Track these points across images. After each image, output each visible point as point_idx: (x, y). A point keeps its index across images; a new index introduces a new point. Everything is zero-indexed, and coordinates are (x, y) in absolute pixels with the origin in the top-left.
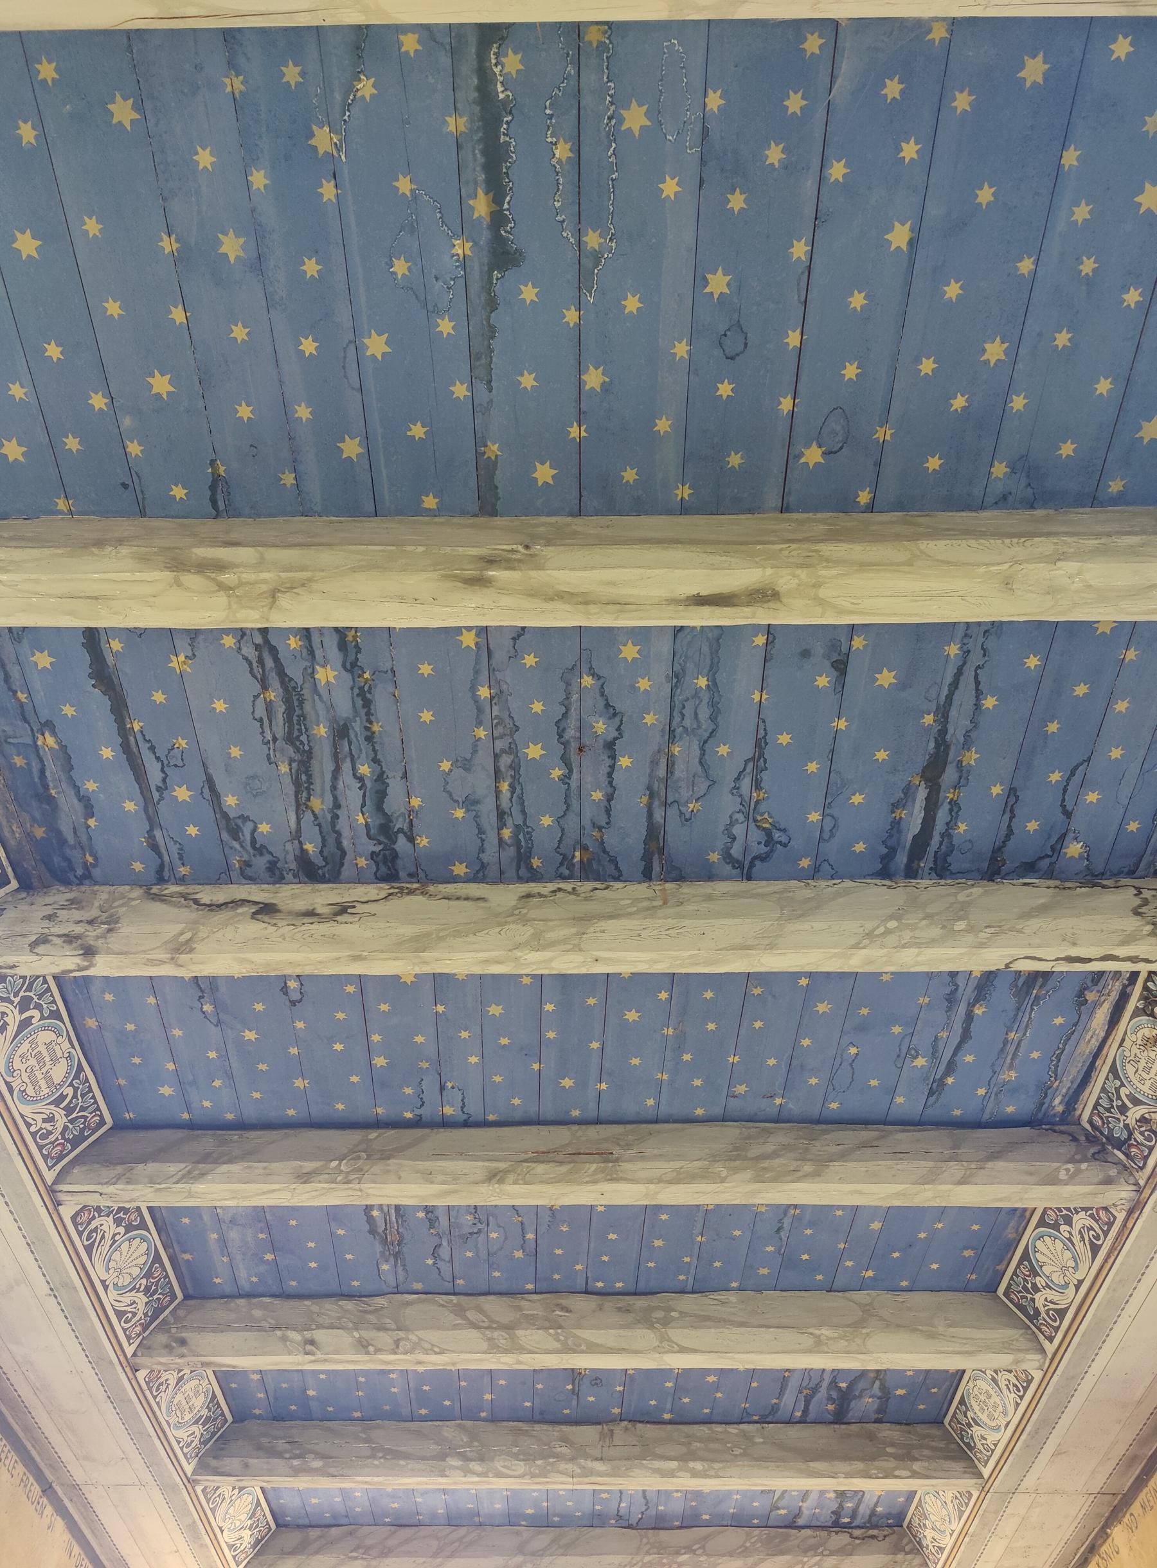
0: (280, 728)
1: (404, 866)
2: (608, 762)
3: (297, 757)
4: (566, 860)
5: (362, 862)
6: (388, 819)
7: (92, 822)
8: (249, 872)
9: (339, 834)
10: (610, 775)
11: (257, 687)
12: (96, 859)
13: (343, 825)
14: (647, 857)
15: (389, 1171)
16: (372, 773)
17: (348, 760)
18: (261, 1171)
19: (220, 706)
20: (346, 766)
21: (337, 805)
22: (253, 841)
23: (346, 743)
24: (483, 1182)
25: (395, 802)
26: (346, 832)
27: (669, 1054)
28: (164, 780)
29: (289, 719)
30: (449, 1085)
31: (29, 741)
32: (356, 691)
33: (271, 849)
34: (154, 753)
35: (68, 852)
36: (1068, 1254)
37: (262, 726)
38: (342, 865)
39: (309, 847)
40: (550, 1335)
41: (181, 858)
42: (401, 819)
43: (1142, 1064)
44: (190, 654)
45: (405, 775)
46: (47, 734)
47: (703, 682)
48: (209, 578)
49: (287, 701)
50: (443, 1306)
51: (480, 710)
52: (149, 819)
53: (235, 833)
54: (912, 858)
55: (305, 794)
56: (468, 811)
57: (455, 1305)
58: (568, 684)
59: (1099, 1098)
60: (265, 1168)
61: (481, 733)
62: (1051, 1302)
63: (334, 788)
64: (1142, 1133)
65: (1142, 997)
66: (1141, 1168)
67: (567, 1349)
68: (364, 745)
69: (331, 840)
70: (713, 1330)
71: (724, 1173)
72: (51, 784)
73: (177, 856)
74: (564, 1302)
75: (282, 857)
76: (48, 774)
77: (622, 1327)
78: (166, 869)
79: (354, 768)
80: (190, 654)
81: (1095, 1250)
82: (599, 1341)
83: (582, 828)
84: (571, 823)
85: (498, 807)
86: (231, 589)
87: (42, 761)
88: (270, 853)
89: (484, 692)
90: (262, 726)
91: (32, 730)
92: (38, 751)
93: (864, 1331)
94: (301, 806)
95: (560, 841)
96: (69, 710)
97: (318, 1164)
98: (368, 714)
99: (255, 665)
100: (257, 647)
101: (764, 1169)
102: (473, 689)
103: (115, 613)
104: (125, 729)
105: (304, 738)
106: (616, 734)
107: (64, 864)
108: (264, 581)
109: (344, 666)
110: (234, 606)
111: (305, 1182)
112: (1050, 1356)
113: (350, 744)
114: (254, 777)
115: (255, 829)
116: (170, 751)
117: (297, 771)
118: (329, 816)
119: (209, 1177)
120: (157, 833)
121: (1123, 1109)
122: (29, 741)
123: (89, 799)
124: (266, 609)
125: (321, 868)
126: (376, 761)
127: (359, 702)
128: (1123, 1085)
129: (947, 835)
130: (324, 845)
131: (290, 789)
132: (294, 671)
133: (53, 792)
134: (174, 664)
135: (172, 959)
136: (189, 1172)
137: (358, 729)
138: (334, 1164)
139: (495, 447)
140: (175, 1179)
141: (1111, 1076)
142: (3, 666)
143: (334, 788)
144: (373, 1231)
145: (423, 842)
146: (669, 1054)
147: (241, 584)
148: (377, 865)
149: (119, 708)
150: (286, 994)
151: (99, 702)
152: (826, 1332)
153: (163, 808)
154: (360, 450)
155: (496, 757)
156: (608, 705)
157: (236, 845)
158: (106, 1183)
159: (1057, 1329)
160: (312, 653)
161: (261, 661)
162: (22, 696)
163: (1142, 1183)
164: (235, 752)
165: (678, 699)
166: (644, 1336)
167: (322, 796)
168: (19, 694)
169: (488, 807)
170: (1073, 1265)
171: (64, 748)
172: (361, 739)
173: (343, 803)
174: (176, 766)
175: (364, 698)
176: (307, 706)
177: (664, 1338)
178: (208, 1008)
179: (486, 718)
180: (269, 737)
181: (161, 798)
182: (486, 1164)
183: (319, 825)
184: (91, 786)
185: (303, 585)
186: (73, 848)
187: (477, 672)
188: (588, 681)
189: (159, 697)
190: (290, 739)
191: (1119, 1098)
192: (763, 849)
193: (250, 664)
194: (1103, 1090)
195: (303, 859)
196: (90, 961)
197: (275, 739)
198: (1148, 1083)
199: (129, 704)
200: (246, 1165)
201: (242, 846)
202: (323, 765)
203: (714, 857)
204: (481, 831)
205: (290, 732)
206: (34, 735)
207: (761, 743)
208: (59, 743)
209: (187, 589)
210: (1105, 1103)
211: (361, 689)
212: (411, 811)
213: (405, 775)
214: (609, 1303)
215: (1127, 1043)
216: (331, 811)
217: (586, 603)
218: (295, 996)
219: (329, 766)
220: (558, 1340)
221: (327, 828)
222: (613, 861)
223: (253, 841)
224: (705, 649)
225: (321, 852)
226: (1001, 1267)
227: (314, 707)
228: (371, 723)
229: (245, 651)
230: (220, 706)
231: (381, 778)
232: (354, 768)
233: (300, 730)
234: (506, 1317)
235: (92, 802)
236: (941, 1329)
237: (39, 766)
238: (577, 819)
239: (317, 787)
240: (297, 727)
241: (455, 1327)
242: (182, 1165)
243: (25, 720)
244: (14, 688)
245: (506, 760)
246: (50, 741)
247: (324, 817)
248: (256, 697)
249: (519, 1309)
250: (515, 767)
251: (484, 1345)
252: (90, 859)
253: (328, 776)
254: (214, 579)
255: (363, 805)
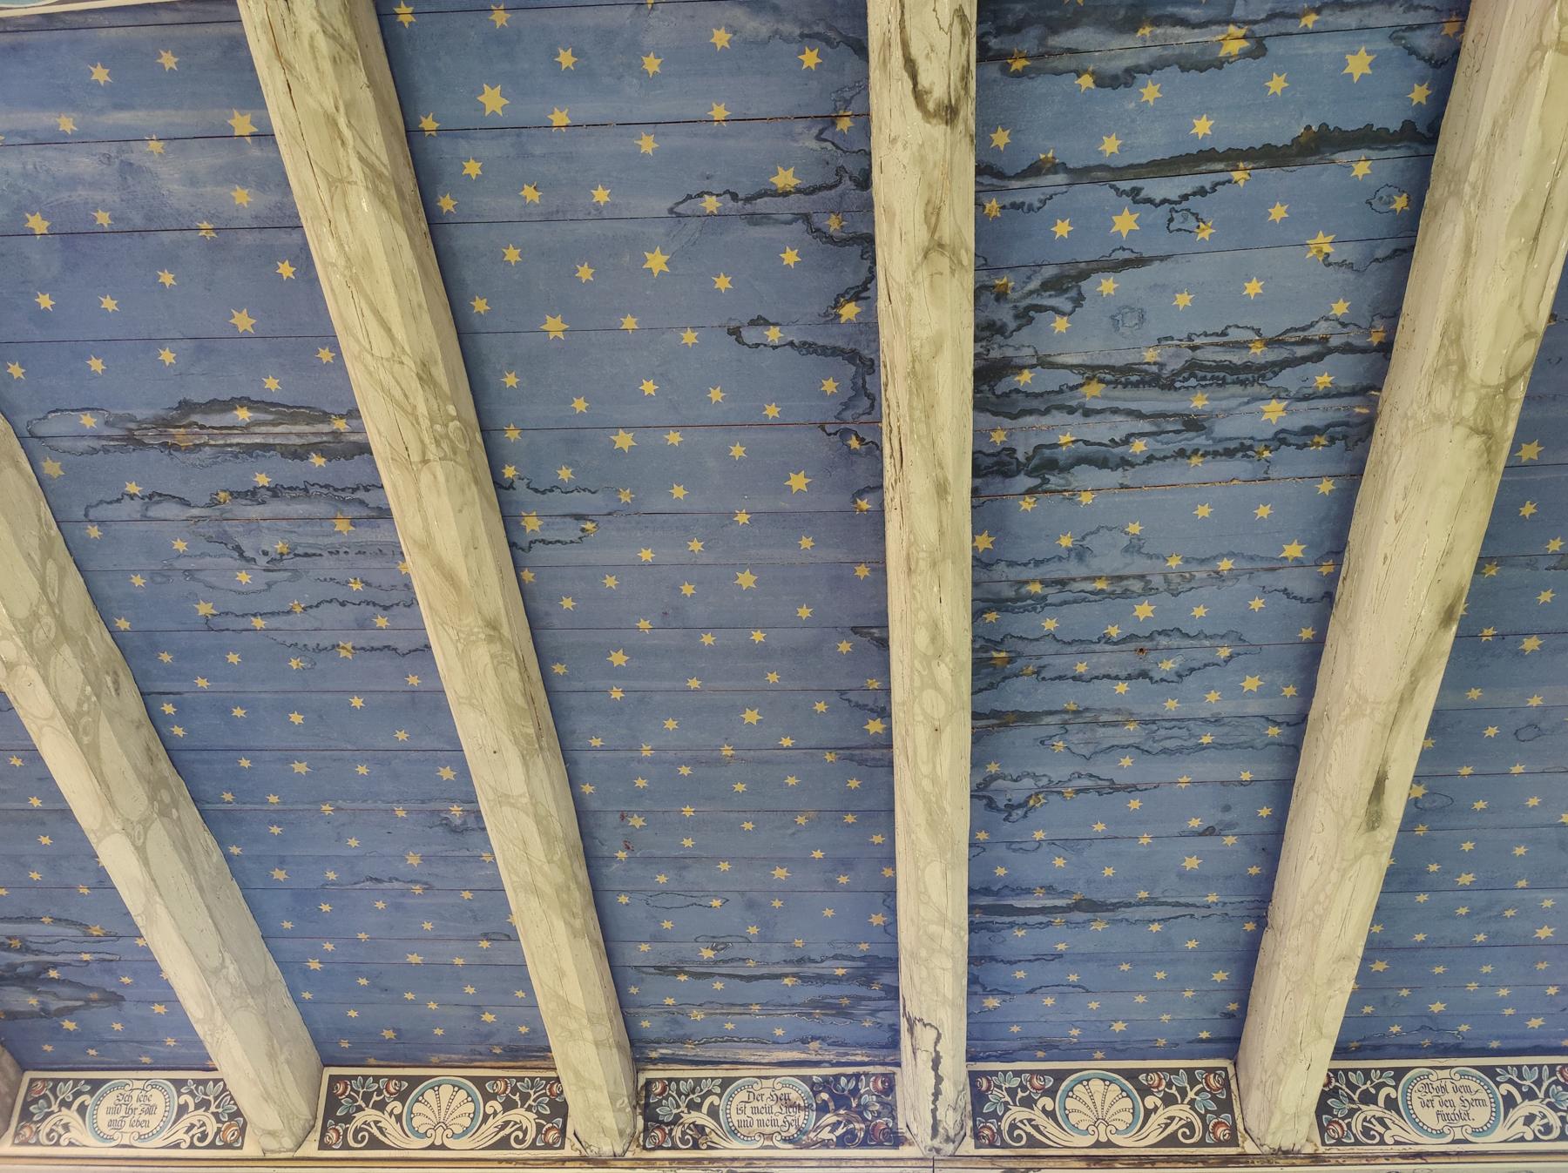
0: (1209, 355)
1: (996, 484)
2: (1124, 674)
3: (1166, 372)
4: (997, 645)
5: (999, 437)
6: (1066, 469)
7: (1086, 81)
8: (988, 297)
9: (1046, 412)
10: (1108, 677)
11: (1269, 333)
12: (1018, 75)
13: (1058, 417)
14: (995, 714)
15: (463, 491)
16: (1134, 455)
17: (1154, 429)
18: (415, 303)
19: (1253, 288)
20: (1145, 426)
21: (1088, 413)
22: (1040, 309)
23: (1180, 427)
24: (484, 619)
25: (1086, 476)
26: (1046, 421)
27: (688, 754)
28: (1149, 201)
29: (1220, 366)
30: (589, 526)
31: (1238, 12)
32: (1248, 442)
33: (1025, 330)
34: (1194, 194)
35: (1033, 32)
36: (467, 1122)
37: (1217, 334)
38: (995, 414)
39: (1025, 378)
40: (83, 690)
41: (1014, 206)
42: (1062, 482)
43: (760, 1104)
44: (1331, 259)
45: (1123, 487)
46: (1245, 44)
47: (1206, 740)
48: (1525, 369)
49: (1247, 367)
50: (40, 520)
51: (1202, 561)
52: (1087, 170)
53: (1055, 285)
54: (989, 906)
55: (1109, 377)
56: (1069, 550)
57: (49, 537)
58: (1223, 637)
59: (686, 1080)
60: (420, 306)
61: (1174, 562)
62: (380, 1129)
63: (1115, 411)
64: (684, 1133)
65: (826, 1079)
66: (644, 1148)
67: (74, 723)
68: (1176, 447)
69: (1035, 404)
70: (181, 866)
71: (556, 858)
72: (1159, 31)
73: (1019, 200)
74: (122, 678)
75: (1009, 341)
76: (1178, 30)
77: (135, 767)
78: (995, 181)
79: (1142, 435)
80: (1331, 259)
81: (503, 1144)
82: (104, 753)
83: (1039, 657)
84: (1048, 647)
85: (1074, 580)
86: (1506, 390)
87: (1194, 26)
88: (1019, 328)
89: (1225, 565)
90: (1217, 334)
91: (1255, 22)
92: (1218, 23)
93: (250, 1001)
94: (1091, 372)
95: (1021, 638)
96: (1277, 84)
97: (446, 387)
98: (1215, 454)
99: (1302, 334)
100: (1325, 340)
101: (569, 888)
102: (1231, 555)
103: (1510, 258)
104: (1238, 160)
105: (1193, 382)
106: (1157, 678)
107: (1010, 19)
108: (1505, 425)
109: (1283, 431)
110: (1483, 391)
111: (420, 378)
112: (299, 1153)
113: (1177, 432)
114: (1142, 318)
115: (1063, 314)
116: (1196, 215)
117: (1146, 372)
118: (1074, 403)
119: (384, 215)
120: (1061, 178)
121: (694, 1106)
122: (1238, 12)
123: (1127, 85)
124: (1471, 423)
125: (992, 390)
126: (1150, 459)
127: (1232, 445)
128: (720, 1096)
129: (1012, 925)
130: (1027, 395)
131: (1118, 360)
132: (1288, 378)
133: (1146, 31)
134: (1320, 238)
135: (941, 245)
136: (380, 176)
137: (1196, 441)
138: (452, 410)
139: (1493, 573)
140: (365, 152)
141: (719, 1082)
142: (1361, 5)
143: (1115, 411)
144: (186, 407)
145: (1027, 504)
146: (688, 754)
147: (1508, 402)
148: (993, 455)
149: (1270, 156)
150: (753, 323)
151: (1285, 130)
152: (232, 969)
153: (1104, 193)
154: (1524, 459)
155: (1142, 577)
156: (1192, 670)
157: (1034, 284)
158: (321, 15)
159: (346, 1147)
160: (1306, 398)
161: (1305, 342)
162: (1309, 21)
163: (629, 1155)
164: (1183, 300)
165: (1192, 724)
166: (135, 800)
167: (1104, 397)
168: (1314, 17)
169: (1073, 569)
170: (458, 1130)
171: (1219, 64)
172: (1182, 445)
173: (1089, 420)
174: (1171, 220)
175: (1241, 449)
176: (1238, 389)
177: (145, 822)
178: (711, 204)
179: (1194, 567)
180: (1198, 341)
181: (1120, 193)
182: (503, 612)
183: (1061, 391)
184: (1150, 91)
185: (1489, 462)
186: (1042, 40)
187: (1252, 558)
188: (1224, 653)
189: (1278, 212)
190: (1193, 368)
191: (704, 1097)
192: (1001, 802)
193: (1303, 329)
194: (698, 1081)
195: (1007, 367)
196: (936, 114)
197: (1194, 348)
198: (743, 1117)
199: (1275, 170)
200: (416, 271)
201: (1031, 293)
202: (1152, 400)
203: (993, 768)
204: (1038, 563)
205: (1202, 367)
206: (1245, 23)
207: (1131, 789)
208: (1228, 59)
209: (1518, 344)
210: (683, 1087)
211: (1251, 448)
212: (1075, 492)
213: (1123, 487)
214: (148, 731)
215: (768, 1083)
216: (1081, 406)
217: (1401, 701)
218: (750, 335)
219: (1146, 407)
220: (80, 705)
221: (1057, 400)
222: (992, 686)
223: (1040, 309)
224: (1243, 739)
225: (1017, 391)
226: (372, 1061)
227: (1233, 396)
228: (1203, 456)
229: (1323, 324)
230: (1253, 288)
231: (1125, 463)
232: (1142, 435)
233: (1204, 378)
234: (73, 621)
235: (1122, 89)
236: (282, 1058)
237: (1193, 19)
238: (1051, 651)
239: (1119, 392)
240: (1209, 375)
241: (28, 557)
242: (385, 158)
243: (1271, 17)
244: (1326, 12)
245: (1137, 586)
246: (1234, 47)
247: (1072, 398)
248: (1258, 332)
249: (88, 629)
250: (1126, 594)
251: (22, 612)
252: (1018, 65)
253: (1134, 406)
254: (1522, 374)
255: (1086, 443)
